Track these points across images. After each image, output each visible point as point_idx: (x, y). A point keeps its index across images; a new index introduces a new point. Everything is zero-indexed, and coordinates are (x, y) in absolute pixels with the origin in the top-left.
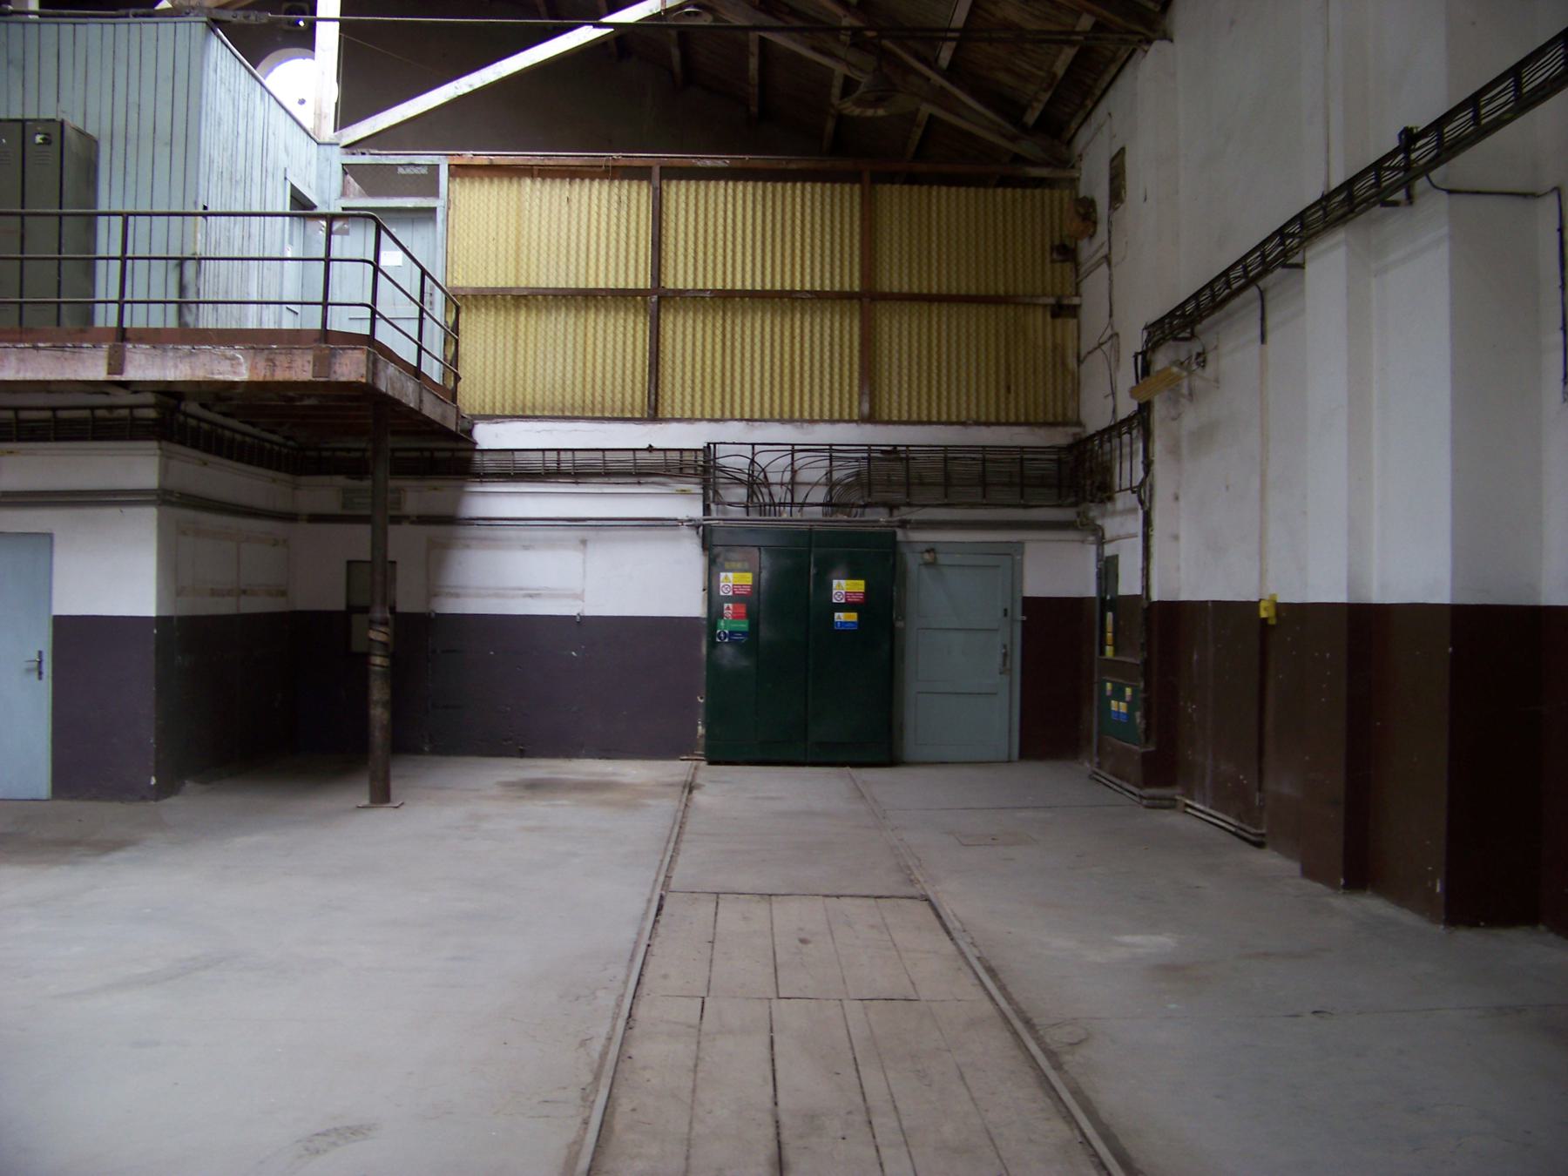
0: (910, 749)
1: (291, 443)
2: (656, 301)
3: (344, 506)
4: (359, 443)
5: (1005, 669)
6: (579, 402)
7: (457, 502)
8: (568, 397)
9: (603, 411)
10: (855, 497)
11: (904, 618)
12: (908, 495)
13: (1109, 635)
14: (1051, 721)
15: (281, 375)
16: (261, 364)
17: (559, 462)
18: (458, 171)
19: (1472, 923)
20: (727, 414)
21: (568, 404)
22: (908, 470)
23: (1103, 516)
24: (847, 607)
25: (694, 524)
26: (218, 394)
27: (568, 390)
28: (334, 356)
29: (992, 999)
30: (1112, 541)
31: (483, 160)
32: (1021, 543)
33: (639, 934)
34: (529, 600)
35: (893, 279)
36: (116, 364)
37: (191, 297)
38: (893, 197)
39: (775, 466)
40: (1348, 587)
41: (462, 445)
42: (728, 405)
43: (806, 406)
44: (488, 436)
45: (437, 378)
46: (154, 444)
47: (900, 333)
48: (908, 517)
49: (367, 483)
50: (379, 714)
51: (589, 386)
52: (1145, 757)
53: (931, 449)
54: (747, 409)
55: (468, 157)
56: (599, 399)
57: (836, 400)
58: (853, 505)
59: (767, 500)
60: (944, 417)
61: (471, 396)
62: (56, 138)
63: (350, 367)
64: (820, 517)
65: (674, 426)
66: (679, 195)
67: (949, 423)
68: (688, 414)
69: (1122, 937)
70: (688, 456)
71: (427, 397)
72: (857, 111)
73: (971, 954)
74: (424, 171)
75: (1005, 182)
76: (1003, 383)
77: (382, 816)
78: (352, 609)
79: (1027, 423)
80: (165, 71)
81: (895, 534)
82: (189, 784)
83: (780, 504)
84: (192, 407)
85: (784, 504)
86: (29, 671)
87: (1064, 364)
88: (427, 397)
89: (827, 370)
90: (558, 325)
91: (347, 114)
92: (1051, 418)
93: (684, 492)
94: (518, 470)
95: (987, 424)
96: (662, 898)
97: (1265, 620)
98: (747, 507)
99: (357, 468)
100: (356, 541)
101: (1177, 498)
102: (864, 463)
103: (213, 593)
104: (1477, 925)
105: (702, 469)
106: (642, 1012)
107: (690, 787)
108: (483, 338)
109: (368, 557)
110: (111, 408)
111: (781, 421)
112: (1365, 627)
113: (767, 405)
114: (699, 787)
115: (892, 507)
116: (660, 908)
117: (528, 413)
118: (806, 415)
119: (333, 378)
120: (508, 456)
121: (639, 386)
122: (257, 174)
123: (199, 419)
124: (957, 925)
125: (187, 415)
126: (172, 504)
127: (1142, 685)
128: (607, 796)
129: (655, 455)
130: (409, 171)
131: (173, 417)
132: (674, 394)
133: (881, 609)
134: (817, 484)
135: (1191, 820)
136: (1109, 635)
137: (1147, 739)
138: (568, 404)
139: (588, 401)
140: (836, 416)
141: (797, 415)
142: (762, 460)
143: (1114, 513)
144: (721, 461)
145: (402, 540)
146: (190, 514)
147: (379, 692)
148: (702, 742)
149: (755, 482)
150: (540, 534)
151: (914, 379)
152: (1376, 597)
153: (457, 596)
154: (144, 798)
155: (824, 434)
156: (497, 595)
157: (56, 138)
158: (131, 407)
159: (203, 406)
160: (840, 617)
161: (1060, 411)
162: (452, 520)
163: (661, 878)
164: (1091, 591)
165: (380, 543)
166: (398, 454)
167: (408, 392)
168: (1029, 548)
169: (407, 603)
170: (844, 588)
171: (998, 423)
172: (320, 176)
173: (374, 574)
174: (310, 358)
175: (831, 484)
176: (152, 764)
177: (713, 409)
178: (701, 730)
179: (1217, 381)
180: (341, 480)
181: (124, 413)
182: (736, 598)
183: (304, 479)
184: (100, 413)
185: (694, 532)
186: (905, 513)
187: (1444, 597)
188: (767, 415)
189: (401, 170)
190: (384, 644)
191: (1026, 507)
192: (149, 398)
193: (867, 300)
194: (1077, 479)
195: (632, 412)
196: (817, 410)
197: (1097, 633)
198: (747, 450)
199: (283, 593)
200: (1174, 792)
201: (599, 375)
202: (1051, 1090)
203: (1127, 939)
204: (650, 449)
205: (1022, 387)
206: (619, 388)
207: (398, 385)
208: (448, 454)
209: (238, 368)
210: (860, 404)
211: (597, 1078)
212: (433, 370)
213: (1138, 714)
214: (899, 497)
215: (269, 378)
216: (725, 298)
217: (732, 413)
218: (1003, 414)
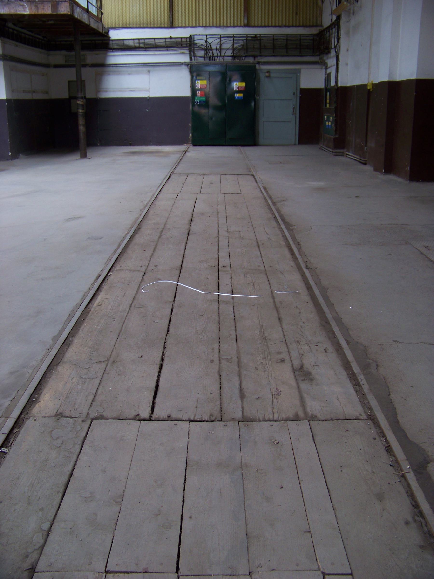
0: (261, 140)
1: (45, 39)
3: (66, 62)
5: (294, 113)
6: (145, 21)
8: (141, 20)
9: (154, 25)
11: (259, 96)
12: (260, 52)
13: (328, 100)
14: (309, 133)
15: (41, 12)
16: (33, 8)
17: (139, 43)
19: (418, 181)
20: (197, 25)
21: (142, 22)
22: (260, 43)
23: (327, 59)
25: (186, 64)
26: (19, 19)
27: (142, 17)
28: (58, 4)
30: (330, 67)
33: (162, 182)
34: (131, 92)
39: (214, 43)
40: (389, 75)
41: (105, 38)
42: (197, 21)
43: (225, 21)
44: (114, 35)
45: (95, 13)
48: (260, 60)
49: (73, 53)
50: (82, 129)
51: (149, 16)
52: (335, 139)
54: (204, 23)
56: (152, 20)
57: (236, 18)
58: (241, 56)
59: (212, 55)
60: (274, 24)
61: (108, 19)
64: (230, 60)
65: (179, 30)
67: (275, 26)
68: (184, 25)
69: (328, 201)
70: (183, 40)
71: (92, 20)
76: (295, 11)
77: (85, 162)
79: (303, 26)
81: (255, 66)
83: (216, 57)
84: (10, 25)
85: (217, 57)
88: (92, 20)
89: (232, 7)
92: (311, 24)
93: (183, 53)
94: (126, 47)
95: (289, 26)
96: (170, 175)
97: (369, 90)
98: (205, 58)
99: (69, 48)
100: (70, 74)
101: (348, 50)
102: (245, 41)
103: (24, 91)
104: (420, 181)
105: (189, 44)
106: (160, 196)
111: (216, 27)
112: (393, 88)
113: (211, 21)
114: (189, 152)
115: (255, 57)
117: (128, 26)
118: (225, 24)
119: (59, 13)
120: (122, 42)
121: (166, 15)
123: (13, 29)
124: (260, 180)
125: (9, 28)
127: (334, 115)
128: (157, 154)
129: (173, 40)
132: (179, 19)
133: (251, 92)
135: (349, 158)
136: (328, 100)
137: (336, 133)
138: (142, 22)
139: (149, 21)
140: (236, 24)
141: (222, 24)
142: (210, 41)
143: (330, 58)
144: (195, 42)
145: (86, 73)
147: (81, 121)
148: (191, 139)
149: (207, 49)
150: (134, 69)
151: (263, 10)
152: (398, 78)
153: (107, 92)
154: (7, 160)
155: (231, 31)
156: (120, 91)
159: (14, 24)
160: (237, 95)
161: (315, 21)
163: (171, 171)
164: (323, 86)
165: (79, 74)
166: (83, 42)
167: (85, 18)
168: (303, 71)
169: (89, 95)
170: (237, 85)
171: (293, 26)
173: (78, 85)
174: (50, 5)
175: (234, 49)
176: (9, 148)
177: (192, 23)
178: (190, 135)
179: (361, 7)
180: (64, 52)
182: (201, 89)
183: (52, 52)
185: (186, 67)
186: (259, 59)
187: (414, 77)
188: (211, 25)
190: (83, 105)
194: (320, 45)
195: (164, 24)
196: (229, 22)
197: (324, 99)
198: (204, 38)
199: (47, 93)
200: (345, 151)
201: (152, 11)
203: (309, 183)
204: (171, 38)
205: (301, 13)
206: (159, 16)
207: (81, 15)
208: (101, 42)
210: (244, 20)
211: (145, 207)
212: (93, 10)
213: (333, 125)
214: (257, 53)
215: (36, 13)
217: (199, 24)
218: (294, 23)
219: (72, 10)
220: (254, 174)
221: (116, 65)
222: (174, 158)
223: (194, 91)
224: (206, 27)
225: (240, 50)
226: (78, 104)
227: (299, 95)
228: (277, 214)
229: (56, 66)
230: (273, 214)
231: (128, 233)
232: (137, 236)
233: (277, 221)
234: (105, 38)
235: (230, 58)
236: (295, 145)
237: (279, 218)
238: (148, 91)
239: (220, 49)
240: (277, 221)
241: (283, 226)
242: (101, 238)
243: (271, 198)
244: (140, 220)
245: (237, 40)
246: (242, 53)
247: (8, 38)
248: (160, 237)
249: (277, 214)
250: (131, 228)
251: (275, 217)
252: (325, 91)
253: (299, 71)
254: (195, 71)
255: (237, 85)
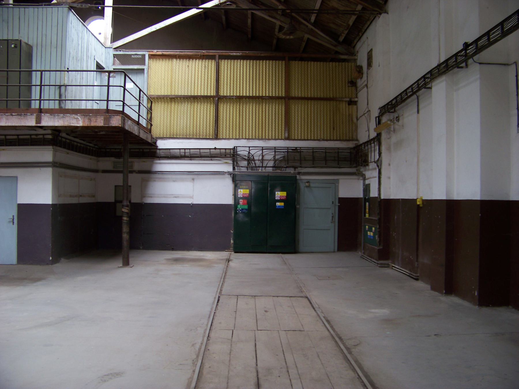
0: (301, 248)
1: (96, 147)
2: (217, 99)
3: (114, 167)
4: (119, 147)
5: (333, 221)
6: (192, 133)
7: (151, 166)
8: (188, 131)
9: (199, 136)
10: (283, 164)
11: (299, 205)
12: (301, 164)
13: (367, 210)
14: (348, 238)
15: (93, 124)
16: (87, 120)
17: (185, 153)
18: (151, 57)
19: (487, 305)
20: (241, 137)
21: (188, 134)
22: (300, 155)
23: (365, 171)
24: (280, 201)
25: (230, 173)
26: (72, 130)
27: (188, 129)
28: (111, 118)
29: (328, 330)
30: (368, 179)
31: (160, 53)
32: (338, 180)
33: (212, 309)
34: (175, 199)
35: (295, 92)
36: (38, 120)
37: (63, 98)
38: (296, 65)
39: (257, 154)
40: (446, 194)
41: (153, 147)
42: (241, 134)
43: (267, 134)
44: (162, 144)
45: (145, 125)
46: (51, 147)
47: (298, 110)
48: (300, 171)
49: (121, 160)
50: (125, 236)
51: (195, 128)
52: (379, 250)
53: (308, 148)
54: (247, 135)
55: (155, 52)
56: (198, 132)
57: (277, 132)
58: (282, 167)
59: (254, 165)
60: (313, 138)
61: (156, 131)
62: (18, 46)
63: (116, 121)
64: (271, 171)
65: (223, 141)
66: (225, 64)
67: (314, 140)
68: (228, 137)
69: (371, 310)
70: (228, 151)
71: (141, 131)
72: (284, 37)
73: (321, 315)
74: (140, 57)
75: (333, 60)
76: (332, 127)
77: (126, 270)
78: (116, 202)
79: (340, 140)
80: (55, 23)
81: (296, 176)
82: (62, 259)
83: (258, 167)
84: (64, 135)
85: (260, 167)
86: (10, 222)
87: (352, 120)
88: (141, 131)
89: (274, 122)
90: (185, 108)
91: (115, 38)
92: (348, 138)
93: (226, 163)
94: (172, 155)
95: (327, 140)
96: (219, 297)
97: (419, 205)
98: (247, 168)
99: (118, 155)
100: (118, 179)
101: (389, 165)
102: (286, 153)
103: (71, 196)
104: (489, 306)
105: (232, 155)
106: (212, 335)
107: (229, 260)
108: (160, 112)
109: (122, 184)
110: (37, 135)
111: (259, 139)
112: (452, 207)
113: (254, 134)
114: (231, 260)
115: (295, 168)
116: (218, 300)
117: (175, 136)
118: (267, 137)
119: (110, 125)
120: (168, 151)
121: (211, 128)
122: (85, 57)
123: (66, 139)
124: (317, 306)
125: (62, 137)
126: (57, 167)
127: (378, 227)
128: (201, 263)
129: (217, 150)
130: (135, 56)
131: (57, 138)
132: (223, 130)
133: (292, 201)
134: (270, 160)
135: (394, 271)
136: (367, 210)
137: (380, 244)
138: (188, 134)
139: (195, 133)
140: (277, 137)
141: (264, 137)
142: (252, 152)
143: (369, 170)
144: (239, 153)
145: (133, 178)
146: (63, 170)
147: (125, 229)
148: (232, 245)
149: (250, 159)
150: (179, 177)
151: (303, 125)
152: (456, 198)
153: (151, 197)
154: (48, 264)
155: (273, 144)
156: (165, 197)
157: (18, 46)
158: (43, 135)
159: (67, 134)
160: (278, 204)
161: (351, 136)
162: (150, 172)
163: (219, 291)
164: (361, 195)
165: (126, 180)
166: (132, 150)
167: (135, 130)
168: (340, 181)
169: (135, 199)
170: (279, 194)
171: (330, 140)
172: (106, 58)
173: (124, 190)
174: (103, 118)
175: (275, 160)
176: (50, 253)
177: (236, 135)
178: (232, 241)
179: (403, 126)
180: (113, 159)
181: (41, 136)
182: (244, 198)
183: (101, 159)
184: (33, 137)
185: (230, 176)
186: (299, 170)
187: (478, 198)
188: (254, 137)
189: (133, 56)
190: (127, 213)
191: (340, 168)
192: (49, 132)
193: (287, 99)
194: (357, 158)
195: (209, 136)
196: (270, 136)
197: (363, 209)
198: (247, 149)
199: (94, 196)
200: (389, 262)
201: (198, 124)
202: (348, 361)
203: (373, 310)
204: (215, 148)
205: (338, 128)
206: (205, 128)
207: (132, 127)
208: (148, 150)
209: (79, 122)
210: (285, 133)
211: (198, 356)
212: (143, 122)
213: (377, 236)
214: (298, 164)
215: (89, 125)
216: (240, 98)
217: (242, 137)
218: (332, 137)
253: (15, 179)
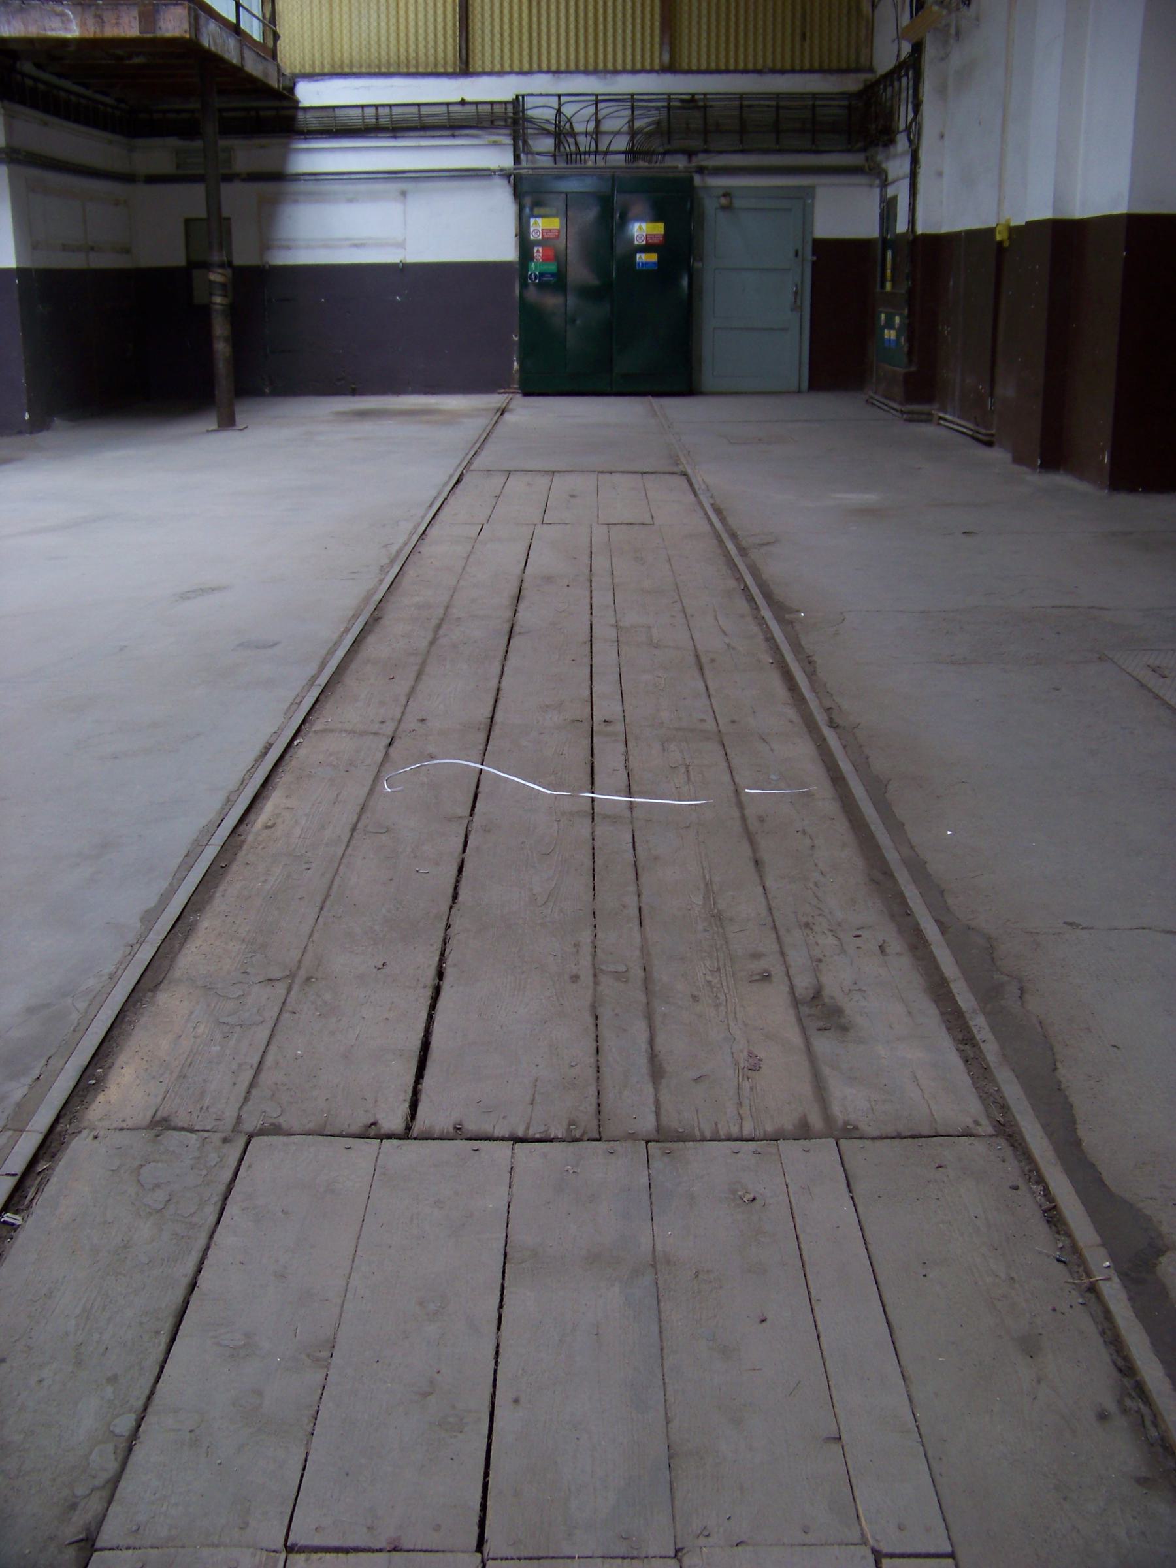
0: (708, 379)
1: (122, 105)
3: (178, 167)
5: (796, 307)
6: (394, 58)
8: (383, 53)
9: (417, 67)
11: (701, 260)
12: (706, 142)
13: (889, 272)
14: (837, 359)
15: (110, 32)
16: (91, 21)
17: (377, 117)
19: (1132, 489)
20: (535, 67)
21: (384, 61)
22: (705, 117)
23: (887, 159)
25: (505, 174)
26: (51, 52)
27: (384, 46)
28: (158, 11)
30: (893, 182)
33: (439, 493)
34: (354, 250)
39: (580, 116)
40: (1054, 202)
41: (285, 104)
42: (535, 58)
43: (610, 57)
44: (310, 94)
45: (257, 35)
48: (704, 163)
49: (198, 144)
50: (222, 348)
51: (402, 42)
52: (907, 377)
54: (554, 61)
56: (413, 54)
57: (638, 50)
58: (653, 153)
59: (573, 149)
60: (741, 66)
61: (294, 51)
64: (623, 164)
65: (485, 80)
67: (745, 71)
68: (497, 68)
69: (889, 544)
70: (497, 109)
71: (248, 54)
76: (798, 31)
77: (229, 438)
79: (821, 71)
81: (691, 180)
83: (585, 153)
84: (28, 67)
85: (589, 153)
88: (248, 54)
89: (629, 20)
92: (844, 65)
93: (495, 144)
94: (341, 127)
95: (782, 72)
96: (462, 474)
97: (1000, 243)
98: (554, 156)
99: (188, 129)
100: (190, 200)
101: (942, 136)
102: (664, 112)
103: (65, 248)
104: (1137, 491)
105: (511, 120)
106: (433, 532)
111: (586, 72)
112: (1064, 237)
113: (572, 57)
114: (511, 411)
115: (690, 154)
117: (347, 70)
118: (610, 66)
119: (159, 34)
120: (330, 113)
121: (450, 40)
123: (36, 80)
124: (703, 487)
125: (23, 75)
127: (906, 311)
128: (425, 418)
129: (468, 108)
132: (484, 50)
133: (681, 250)
135: (945, 428)
136: (889, 272)
137: (910, 361)
138: (384, 61)
139: (403, 58)
140: (638, 66)
141: (601, 66)
142: (568, 110)
143: (895, 156)
144: (530, 113)
145: (234, 197)
147: (220, 328)
148: (517, 376)
149: (561, 132)
150: (362, 187)
151: (713, 27)
152: (1078, 212)
153: (289, 248)
154: (20, 432)
155: (626, 84)
156: (326, 246)
159: (38, 66)
160: (641, 258)
161: (853, 57)
163: (465, 463)
164: (875, 234)
165: (213, 202)
166: (225, 114)
167: (230, 49)
168: (820, 193)
169: (241, 259)
170: (641, 230)
171: (793, 71)
173: (210, 230)
174: (135, 14)
175: (633, 133)
176: (25, 401)
177: (521, 62)
178: (516, 365)
179: (977, 19)
180: (173, 142)
182: (544, 242)
183: (140, 142)
185: (505, 182)
186: (702, 160)
187: (1122, 209)
188: (572, 67)
190: (224, 285)
194: (866, 123)
195: (445, 66)
196: (620, 61)
197: (879, 269)
198: (554, 102)
199: (127, 251)
200: (934, 409)
201: (412, 30)
203: (839, 495)
204: (463, 102)
205: (817, 34)
206: (431, 43)
207: (219, 41)
208: (273, 113)
210: (661, 54)
211: (392, 562)
212: (253, 28)
213: (902, 339)
214: (695, 143)
215: (99, 35)
217: (539, 65)
218: (798, 62)
219: (196, 26)
220: (690, 472)
221: (316, 176)
222: (473, 428)
223: (525, 245)
224: (558, 72)
225: (650, 135)
226: (211, 282)
227: (809, 257)
228: (749, 580)
229: (152, 179)
230: (740, 579)
231: (347, 630)
232: (371, 639)
233: (751, 599)
234: (285, 104)
235: (622, 157)
236: (799, 391)
237: (755, 591)
238: (401, 245)
239: (597, 134)
240: (751, 599)
241: (766, 613)
242: (275, 645)
243: (734, 536)
244: (378, 597)
245: (641, 108)
246: (656, 144)
247: (23, 102)
248: (432, 643)
249: (749, 580)
250: (356, 617)
251: (746, 589)
252: (879, 246)
253: (810, 192)
254: (528, 193)
255: (641, 230)
